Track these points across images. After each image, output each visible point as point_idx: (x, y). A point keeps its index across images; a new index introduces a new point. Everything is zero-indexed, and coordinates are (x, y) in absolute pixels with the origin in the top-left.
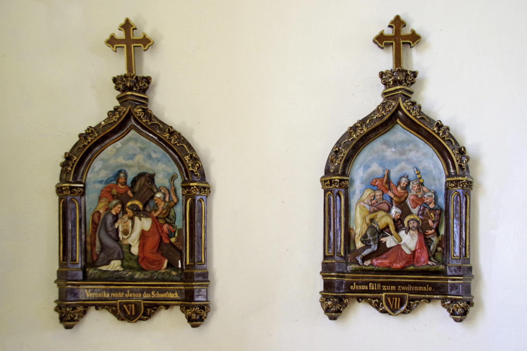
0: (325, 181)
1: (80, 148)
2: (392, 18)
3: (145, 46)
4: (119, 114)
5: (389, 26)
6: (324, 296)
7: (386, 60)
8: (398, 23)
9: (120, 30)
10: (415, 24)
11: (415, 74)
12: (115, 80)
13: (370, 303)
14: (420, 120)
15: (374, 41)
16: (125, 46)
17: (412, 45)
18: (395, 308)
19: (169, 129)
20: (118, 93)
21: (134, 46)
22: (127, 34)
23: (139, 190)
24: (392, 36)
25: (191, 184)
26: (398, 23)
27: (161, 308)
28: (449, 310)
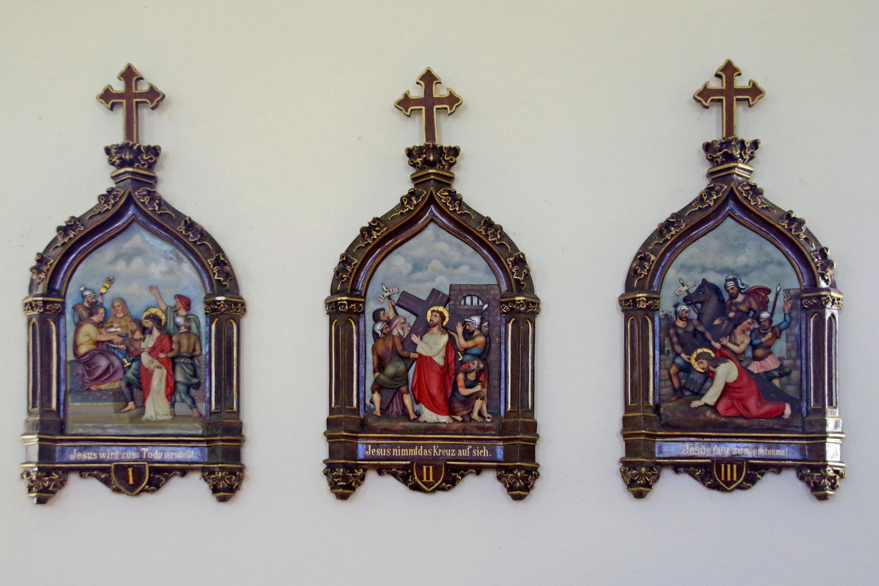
2: (722, 63)
3: (152, 102)
5: (717, 76)
7: (710, 127)
8: (729, 70)
10: (153, 75)
11: (455, 151)
12: (108, 150)
13: (692, 475)
15: (694, 98)
16: (124, 101)
18: (729, 479)
20: (113, 168)
21: (137, 103)
22: (428, 91)
23: (721, 307)
24: (122, 94)
26: (129, 75)
27: (175, 474)
28: (808, 483)
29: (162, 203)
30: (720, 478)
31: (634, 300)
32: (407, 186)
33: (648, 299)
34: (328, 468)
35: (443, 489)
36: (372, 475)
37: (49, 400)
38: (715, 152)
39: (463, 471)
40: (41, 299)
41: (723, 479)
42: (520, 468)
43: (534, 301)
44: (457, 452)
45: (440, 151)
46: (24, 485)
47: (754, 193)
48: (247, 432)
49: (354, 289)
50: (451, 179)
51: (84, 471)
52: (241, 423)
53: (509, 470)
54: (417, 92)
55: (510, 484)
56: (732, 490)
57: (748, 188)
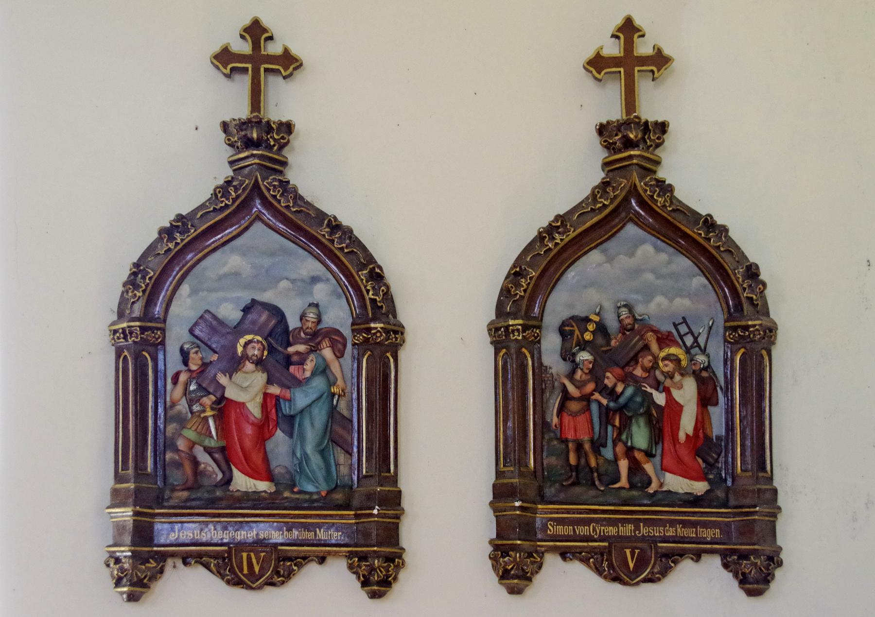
0: (115, 332)
1: (159, 254)
4: (236, 191)
5: (613, 36)
6: (496, 547)
9: (242, 37)
11: (663, 127)
12: (225, 126)
13: (207, 566)
14: (673, 214)
15: (584, 67)
16: (249, 66)
17: (656, 75)
19: (330, 221)
22: (629, 46)
25: (372, 325)
26: (256, 31)
27: (312, 560)
29: (298, 198)
30: (241, 570)
31: (507, 328)
32: (598, 176)
33: (525, 328)
34: (495, 550)
35: (273, 584)
36: (552, 561)
37: (144, 459)
38: (610, 137)
39: (302, 560)
40: (138, 324)
41: (245, 571)
42: (377, 555)
43: (396, 328)
44: (637, 528)
45: (646, 127)
46: (106, 577)
47: (661, 190)
48: (406, 503)
49: (527, 316)
50: (658, 163)
51: (194, 556)
52: (400, 492)
53: (363, 557)
54: (613, 49)
55: (364, 576)
56: (637, 584)
57: (653, 183)
